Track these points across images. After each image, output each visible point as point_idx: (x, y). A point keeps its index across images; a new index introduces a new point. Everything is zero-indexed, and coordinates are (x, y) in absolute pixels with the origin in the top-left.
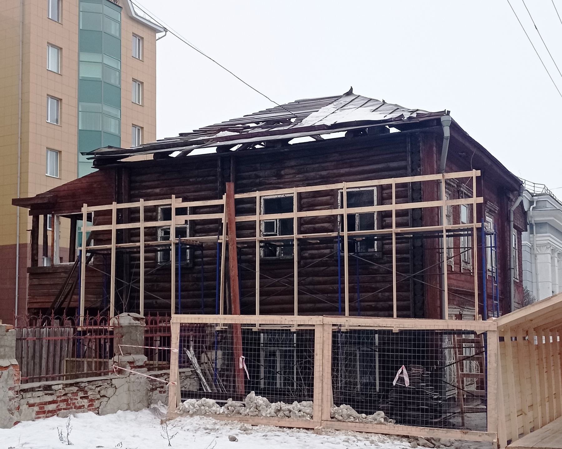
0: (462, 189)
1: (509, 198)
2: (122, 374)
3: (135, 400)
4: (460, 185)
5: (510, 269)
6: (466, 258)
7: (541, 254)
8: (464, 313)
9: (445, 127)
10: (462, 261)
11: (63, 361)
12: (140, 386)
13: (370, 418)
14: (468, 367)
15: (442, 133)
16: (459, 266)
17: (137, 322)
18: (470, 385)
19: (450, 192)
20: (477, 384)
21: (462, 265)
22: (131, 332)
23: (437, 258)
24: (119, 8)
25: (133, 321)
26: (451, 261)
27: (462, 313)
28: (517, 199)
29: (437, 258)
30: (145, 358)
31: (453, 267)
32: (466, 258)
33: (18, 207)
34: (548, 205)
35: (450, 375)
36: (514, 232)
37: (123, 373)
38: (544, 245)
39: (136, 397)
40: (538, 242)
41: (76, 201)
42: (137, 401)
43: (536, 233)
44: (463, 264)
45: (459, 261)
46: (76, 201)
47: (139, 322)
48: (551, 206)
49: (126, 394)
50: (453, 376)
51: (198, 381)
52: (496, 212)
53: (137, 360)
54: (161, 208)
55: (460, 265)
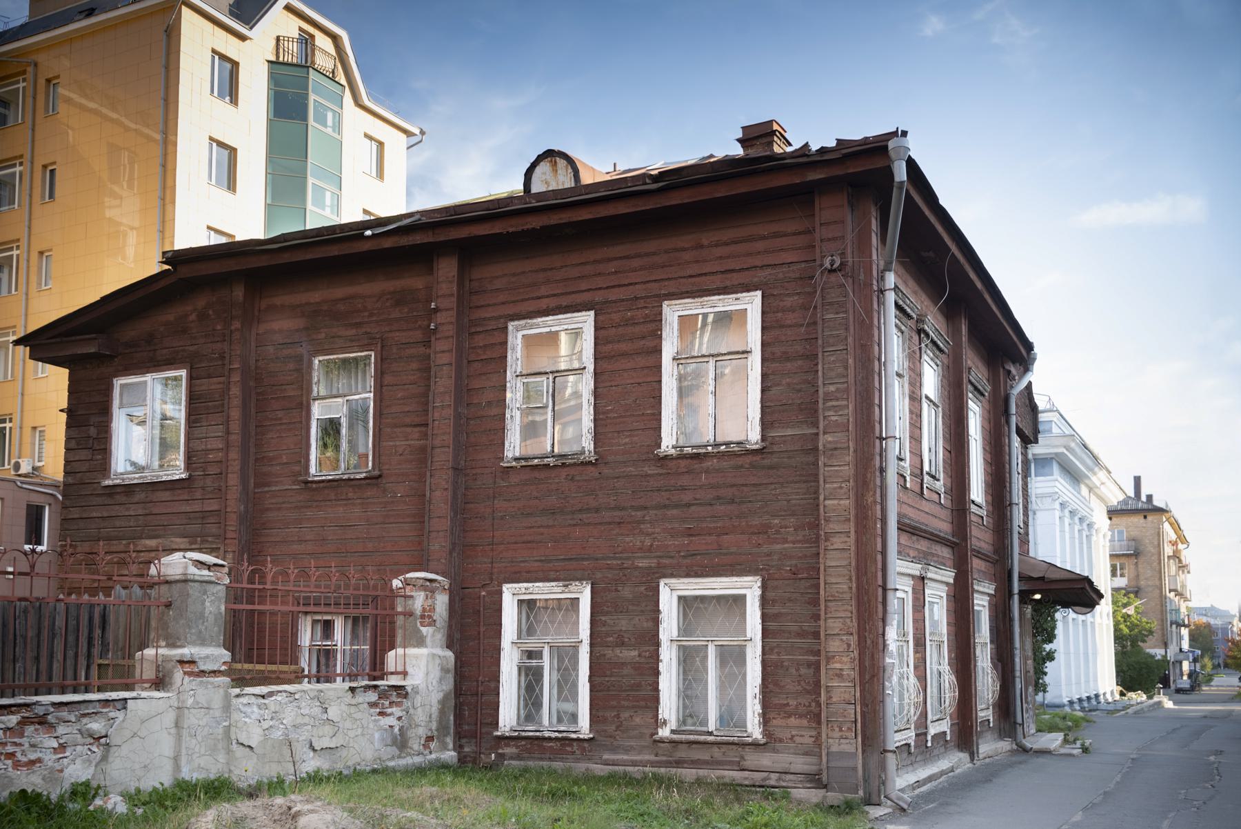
0: (926, 328)
1: (1009, 372)
2: (163, 689)
3: (193, 749)
4: (923, 319)
5: (1011, 504)
6: (933, 469)
7: (1042, 510)
8: (930, 575)
9: (896, 163)
10: (925, 472)
11: (92, 667)
12: (208, 716)
13: (620, 795)
14: (935, 684)
15: (891, 175)
16: (919, 481)
17: (206, 572)
18: (940, 722)
19: (903, 328)
20: (951, 719)
21: (925, 481)
22: (188, 594)
23: (877, 450)
24: (341, 87)
25: (193, 570)
26: (903, 467)
27: (924, 575)
28: (1022, 376)
29: (877, 450)
30: (226, 655)
31: (908, 479)
32: (933, 469)
33: (40, 363)
34: (1055, 430)
35: (901, 698)
36: (1016, 442)
37: (167, 686)
38: (1050, 495)
39: (194, 741)
40: (1039, 491)
41: (155, 350)
42: (197, 750)
43: (1036, 476)
44: (926, 478)
45: (919, 472)
46: (155, 350)
47: (211, 574)
48: (1059, 431)
49: (169, 734)
50: (906, 701)
51: (207, 688)
52: (986, 394)
53: (200, 658)
54: (320, 361)
55: (922, 480)
